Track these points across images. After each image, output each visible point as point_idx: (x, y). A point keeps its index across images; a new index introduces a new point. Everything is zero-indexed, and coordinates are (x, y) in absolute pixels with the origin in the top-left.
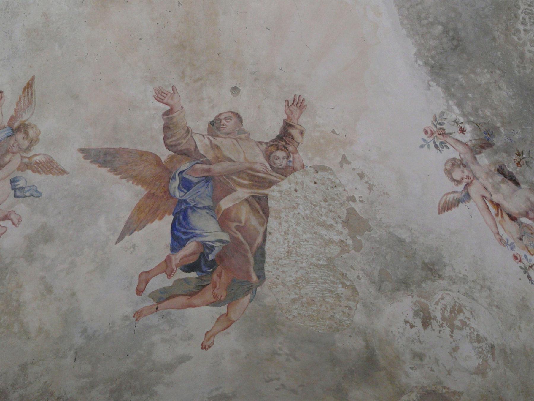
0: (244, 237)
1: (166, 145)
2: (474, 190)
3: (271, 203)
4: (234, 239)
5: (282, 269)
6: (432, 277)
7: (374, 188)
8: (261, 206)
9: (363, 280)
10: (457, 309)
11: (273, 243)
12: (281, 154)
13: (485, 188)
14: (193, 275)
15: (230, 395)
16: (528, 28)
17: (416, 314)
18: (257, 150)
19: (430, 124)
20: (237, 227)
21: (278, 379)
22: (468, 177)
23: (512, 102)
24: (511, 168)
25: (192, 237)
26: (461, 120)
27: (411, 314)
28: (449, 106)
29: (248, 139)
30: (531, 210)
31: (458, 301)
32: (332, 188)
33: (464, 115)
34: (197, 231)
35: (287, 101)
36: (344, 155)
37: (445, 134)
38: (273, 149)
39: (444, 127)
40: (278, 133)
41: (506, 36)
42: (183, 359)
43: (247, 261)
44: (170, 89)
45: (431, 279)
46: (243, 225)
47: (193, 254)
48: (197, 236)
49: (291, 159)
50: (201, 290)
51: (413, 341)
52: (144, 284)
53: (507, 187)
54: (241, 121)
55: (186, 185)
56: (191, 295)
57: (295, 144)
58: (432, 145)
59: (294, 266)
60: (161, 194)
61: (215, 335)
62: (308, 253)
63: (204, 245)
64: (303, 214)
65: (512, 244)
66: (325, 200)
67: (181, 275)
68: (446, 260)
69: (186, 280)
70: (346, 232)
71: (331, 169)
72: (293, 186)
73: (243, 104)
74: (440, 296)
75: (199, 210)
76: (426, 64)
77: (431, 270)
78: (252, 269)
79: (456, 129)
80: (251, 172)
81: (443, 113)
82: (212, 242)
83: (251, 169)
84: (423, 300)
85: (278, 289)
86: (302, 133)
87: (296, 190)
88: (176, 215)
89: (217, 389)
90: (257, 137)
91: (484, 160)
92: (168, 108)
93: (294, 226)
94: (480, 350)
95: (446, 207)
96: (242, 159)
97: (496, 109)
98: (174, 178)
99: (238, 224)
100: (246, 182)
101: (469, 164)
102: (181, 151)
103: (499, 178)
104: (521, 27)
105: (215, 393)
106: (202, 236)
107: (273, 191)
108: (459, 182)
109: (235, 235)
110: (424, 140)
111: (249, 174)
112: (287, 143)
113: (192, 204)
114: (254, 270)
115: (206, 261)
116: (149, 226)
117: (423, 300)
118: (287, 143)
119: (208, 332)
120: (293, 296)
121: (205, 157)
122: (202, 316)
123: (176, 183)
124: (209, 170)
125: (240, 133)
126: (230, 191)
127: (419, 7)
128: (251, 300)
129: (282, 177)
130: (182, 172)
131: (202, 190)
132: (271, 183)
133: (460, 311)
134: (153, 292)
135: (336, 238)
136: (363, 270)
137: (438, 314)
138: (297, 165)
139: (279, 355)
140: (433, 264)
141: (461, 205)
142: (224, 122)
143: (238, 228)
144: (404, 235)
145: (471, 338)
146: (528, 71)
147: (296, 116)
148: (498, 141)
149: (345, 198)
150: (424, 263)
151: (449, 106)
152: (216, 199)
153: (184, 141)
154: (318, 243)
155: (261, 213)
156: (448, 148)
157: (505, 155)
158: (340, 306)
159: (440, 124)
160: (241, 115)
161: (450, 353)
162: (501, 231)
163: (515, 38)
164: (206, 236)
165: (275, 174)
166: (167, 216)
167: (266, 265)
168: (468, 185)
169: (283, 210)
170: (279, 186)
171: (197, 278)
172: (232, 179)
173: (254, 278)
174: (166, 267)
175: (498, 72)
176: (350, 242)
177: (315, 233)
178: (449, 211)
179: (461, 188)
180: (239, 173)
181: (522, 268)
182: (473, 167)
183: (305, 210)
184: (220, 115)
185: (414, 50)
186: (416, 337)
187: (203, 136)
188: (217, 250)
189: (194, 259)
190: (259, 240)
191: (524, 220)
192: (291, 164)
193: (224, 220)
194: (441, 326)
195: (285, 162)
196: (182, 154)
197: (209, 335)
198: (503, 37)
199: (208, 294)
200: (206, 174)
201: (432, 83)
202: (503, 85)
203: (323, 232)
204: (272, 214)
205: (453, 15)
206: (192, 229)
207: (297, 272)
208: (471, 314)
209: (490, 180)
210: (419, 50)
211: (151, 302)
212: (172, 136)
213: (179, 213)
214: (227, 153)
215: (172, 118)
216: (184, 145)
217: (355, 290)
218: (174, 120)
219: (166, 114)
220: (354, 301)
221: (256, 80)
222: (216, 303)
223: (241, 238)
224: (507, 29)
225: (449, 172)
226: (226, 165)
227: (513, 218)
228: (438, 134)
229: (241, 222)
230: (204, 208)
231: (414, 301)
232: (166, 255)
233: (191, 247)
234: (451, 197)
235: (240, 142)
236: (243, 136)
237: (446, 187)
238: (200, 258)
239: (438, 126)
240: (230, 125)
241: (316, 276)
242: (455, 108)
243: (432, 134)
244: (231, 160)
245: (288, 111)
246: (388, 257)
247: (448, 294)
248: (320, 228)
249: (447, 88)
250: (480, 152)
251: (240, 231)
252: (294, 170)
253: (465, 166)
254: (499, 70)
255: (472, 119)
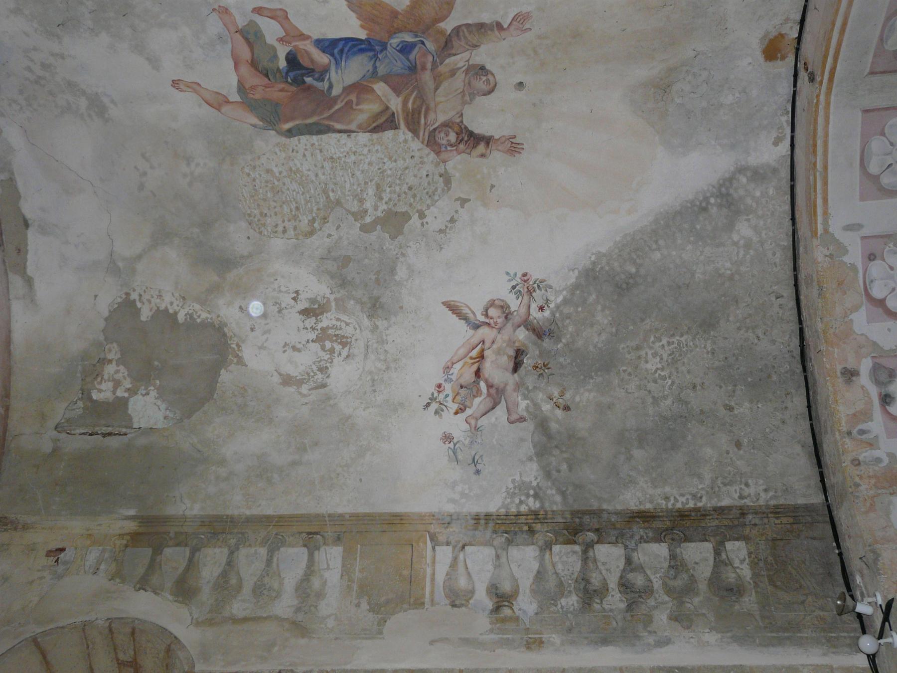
0: (339, 110)
1: (460, 26)
2: (484, 331)
3: (389, 134)
4: (335, 100)
5: (308, 154)
6: (366, 309)
7: (443, 235)
8: (384, 122)
9: (328, 240)
10: (344, 342)
11: (339, 141)
12: (453, 137)
13: (493, 342)
14: (282, 64)
15: (107, 116)
16: (666, 348)
17: (313, 301)
18: (453, 113)
19: (534, 278)
20: (350, 102)
21: (152, 167)
22: (496, 323)
23: (591, 348)
24: (528, 361)
25: (335, 59)
26: (552, 305)
27: (310, 295)
28: (561, 291)
29: (464, 103)
30: (497, 389)
31: (353, 340)
32: (427, 193)
33: (558, 307)
34: (343, 63)
35: (515, 137)
36: (470, 200)
37: (531, 293)
38: (457, 128)
39: (537, 290)
40: (476, 132)
41: (651, 330)
42: (154, 62)
43: (306, 117)
44: (527, 26)
45: (362, 308)
46: (354, 107)
47: (312, 61)
48: (337, 63)
49: (449, 148)
50: (261, 73)
51: (277, 303)
52: (269, 15)
53: (506, 361)
54: (484, 95)
55: (406, 49)
56: (254, 64)
57: (468, 151)
58: (514, 283)
59: (316, 166)
60: (395, 25)
61: (195, 91)
62: (338, 179)
63: (326, 70)
64: (385, 167)
65: (451, 380)
66: (410, 188)
67: (282, 52)
68: (393, 319)
69: (275, 57)
70: (379, 213)
71: (449, 189)
72: (417, 154)
73: (505, 95)
74: (348, 321)
75: (372, 62)
76: (594, 263)
77: (374, 306)
78: (297, 122)
79: (541, 302)
80: (423, 110)
81: (551, 287)
82: (329, 78)
83: (428, 109)
84: (333, 304)
85: (279, 153)
86: (483, 156)
87: (412, 157)
88: (368, 41)
89: (113, 101)
90: (468, 112)
91: (522, 335)
92: (505, 26)
93: (367, 161)
94: (312, 374)
95: (453, 308)
96: (438, 99)
97: (578, 335)
98: (416, 36)
99: (354, 102)
100: (410, 105)
101: (511, 322)
102: (451, 41)
103: (512, 353)
104: (664, 341)
105: (105, 100)
106: (337, 68)
107: (404, 133)
108: (487, 315)
109: (339, 101)
110: (515, 275)
111: (420, 107)
112: (466, 142)
113: (380, 56)
114: (297, 125)
115: (303, 75)
116: (353, 15)
117: (333, 304)
118: (466, 142)
119: (198, 84)
120: (275, 170)
121: (441, 64)
122: (224, 77)
123: (409, 38)
124: (424, 68)
125: (469, 95)
126: (397, 91)
127: (647, 249)
128: (254, 126)
129: (426, 142)
130: (423, 43)
131: (399, 64)
132: (415, 132)
133: (344, 344)
134: (255, 22)
135: (368, 205)
136: (340, 238)
137: (325, 323)
138: (444, 156)
139: (188, 164)
140: (382, 307)
141: (463, 322)
142: (484, 78)
143: (349, 103)
144: (401, 273)
145: (319, 362)
146: (628, 356)
147: (500, 148)
148: (547, 343)
149: (420, 208)
150: (379, 298)
151: (561, 291)
152: (386, 79)
153: (463, 43)
154: (355, 187)
155: (374, 125)
156: (518, 298)
157: (537, 352)
158: (283, 221)
159: (539, 286)
160: (492, 94)
161: (286, 345)
162: (458, 366)
163: (652, 339)
164: (337, 73)
165: (427, 134)
166: (366, 32)
167: (308, 137)
168: (489, 324)
169: (383, 147)
170: (413, 140)
171: (278, 68)
172: (413, 92)
173: (287, 126)
174: (292, 34)
175: (614, 330)
176: (368, 220)
177: (366, 183)
178: (450, 312)
179: (482, 319)
180: (421, 97)
181: (433, 394)
182: (509, 325)
183: (391, 169)
184: (493, 74)
185: (603, 250)
186: (283, 305)
187: (468, 61)
188: (319, 85)
189: (305, 62)
190: (338, 126)
191: (483, 385)
192: (443, 149)
193: (360, 88)
194: (313, 329)
195: (444, 142)
196: (446, 42)
197: (195, 86)
198: (648, 327)
199: (254, 80)
200: (419, 67)
201: (576, 272)
202: (604, 337)
203: (371, 191)
204: (375, 136)
205: (650, 279)
206: (347, 58)
207: (309, 170)
208: (347, 356)
209: (505, 345)
210: (604, 255)
211: (241, 22)
212: (470, 32)
213: (370, 43)
214: (445, 85)
215: (492, 30)
216: (455, 42)
217: (311, 233)
218: (489, 32)
219: (499, 26)
220: (296, 235)
221: (534, 105)
222: (242, 88)
223: (337, 107)
224: (657, 329)
225: (492, 304)
226: (431, 84)
227: (478, 373)
228: (527, 287)
229: (357, 104)
230: (375, 68)
231: (328, 295)
232: (310, 34)
233: (322, 59)
234: (466, 311)
235: (460, 96)
236: (467, 98)
237: (476, 306)
238: (308, 69)
239: (535, 285)
240: (480, 84)
241: (312, 191)
242: (560, 299)
243: (525, 281)
244: (436, 89)
245: (504, 139)
246: (366, 261)
247: (355, 329)
248: (374, 187)
249: (576, 287)
250: (528, 329)
251: (346, 103)
252: (438, 153)
253: (506, 317)
254: (617, 330)
255: (557, 315)
